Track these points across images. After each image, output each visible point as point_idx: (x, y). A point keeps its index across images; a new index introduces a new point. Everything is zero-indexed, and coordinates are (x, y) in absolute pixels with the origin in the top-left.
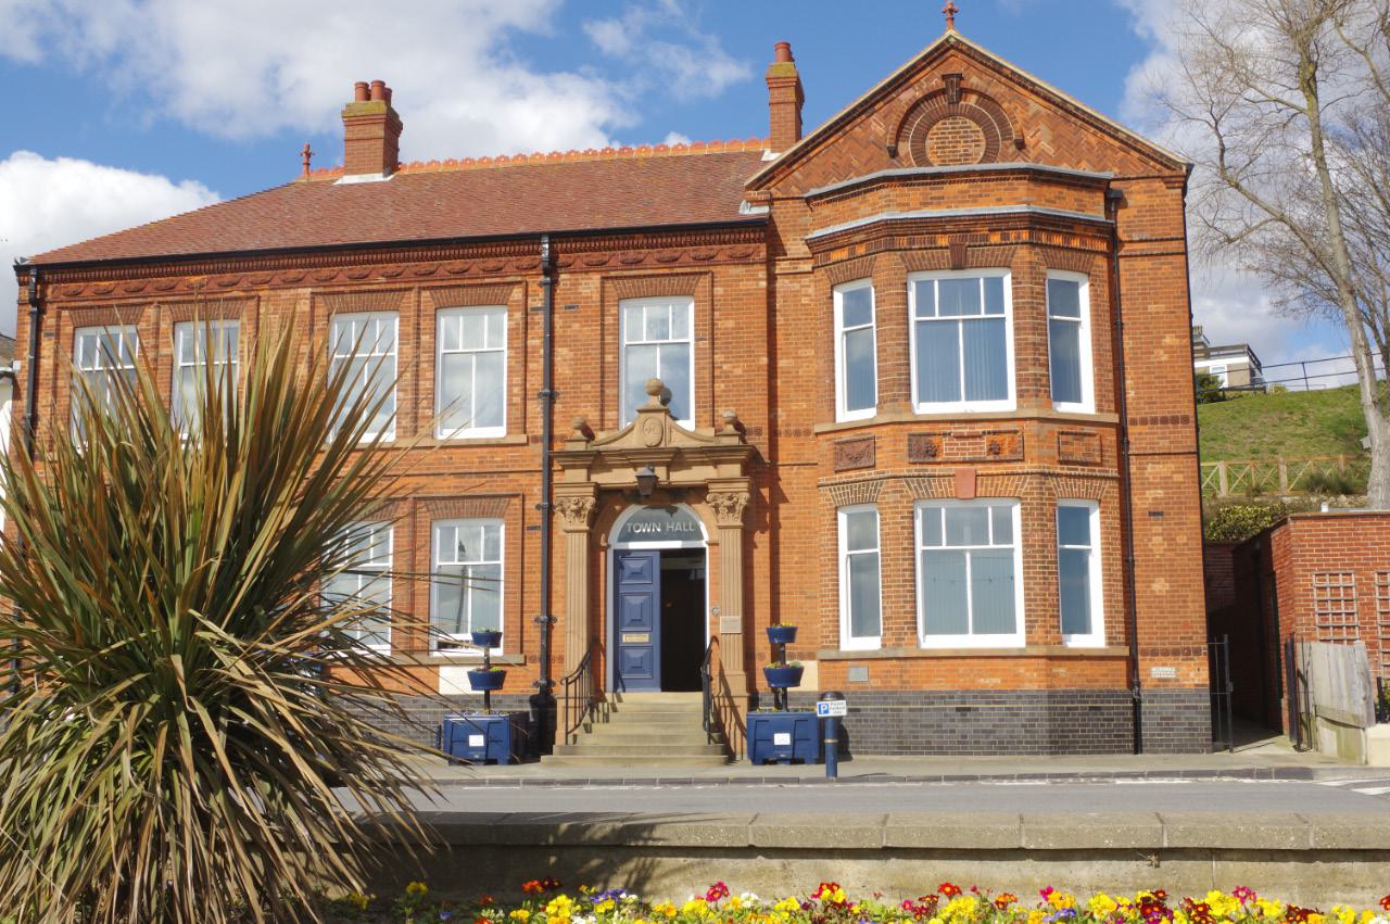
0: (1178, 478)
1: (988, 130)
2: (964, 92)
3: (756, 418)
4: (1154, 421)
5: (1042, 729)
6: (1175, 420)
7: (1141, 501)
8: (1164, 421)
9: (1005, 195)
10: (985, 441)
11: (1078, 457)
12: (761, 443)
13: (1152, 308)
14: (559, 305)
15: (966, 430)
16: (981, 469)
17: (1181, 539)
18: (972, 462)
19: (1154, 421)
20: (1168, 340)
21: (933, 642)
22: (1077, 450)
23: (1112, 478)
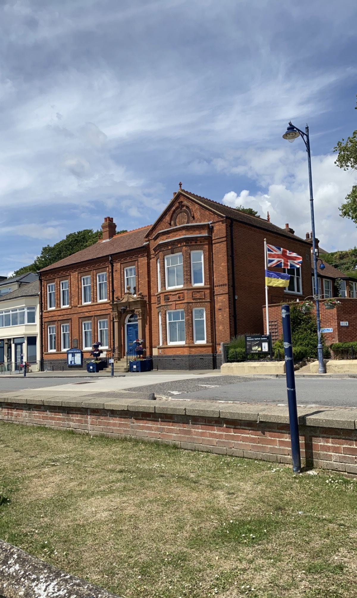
0: (224, 300)
1: (188, 214)
2: (183, 206)
3: (146, 293)
4: (220, 286)
5: (187, 363)
6: (224, 285)
7: (217, 306)
8: (222, 285)
9: (181, 234)
10: (178, 295)
11: (198, 297)
12: (146, 299)
13: (220, 256)
14: (114, 270)
15: (174, 293)
16: (177, 302)
17: (225, 315)
18: (175, 301)
19: (220, 286)
20: (223, 264)
21: (171, 344)
22: (198, 296)
23: (208, 302)
